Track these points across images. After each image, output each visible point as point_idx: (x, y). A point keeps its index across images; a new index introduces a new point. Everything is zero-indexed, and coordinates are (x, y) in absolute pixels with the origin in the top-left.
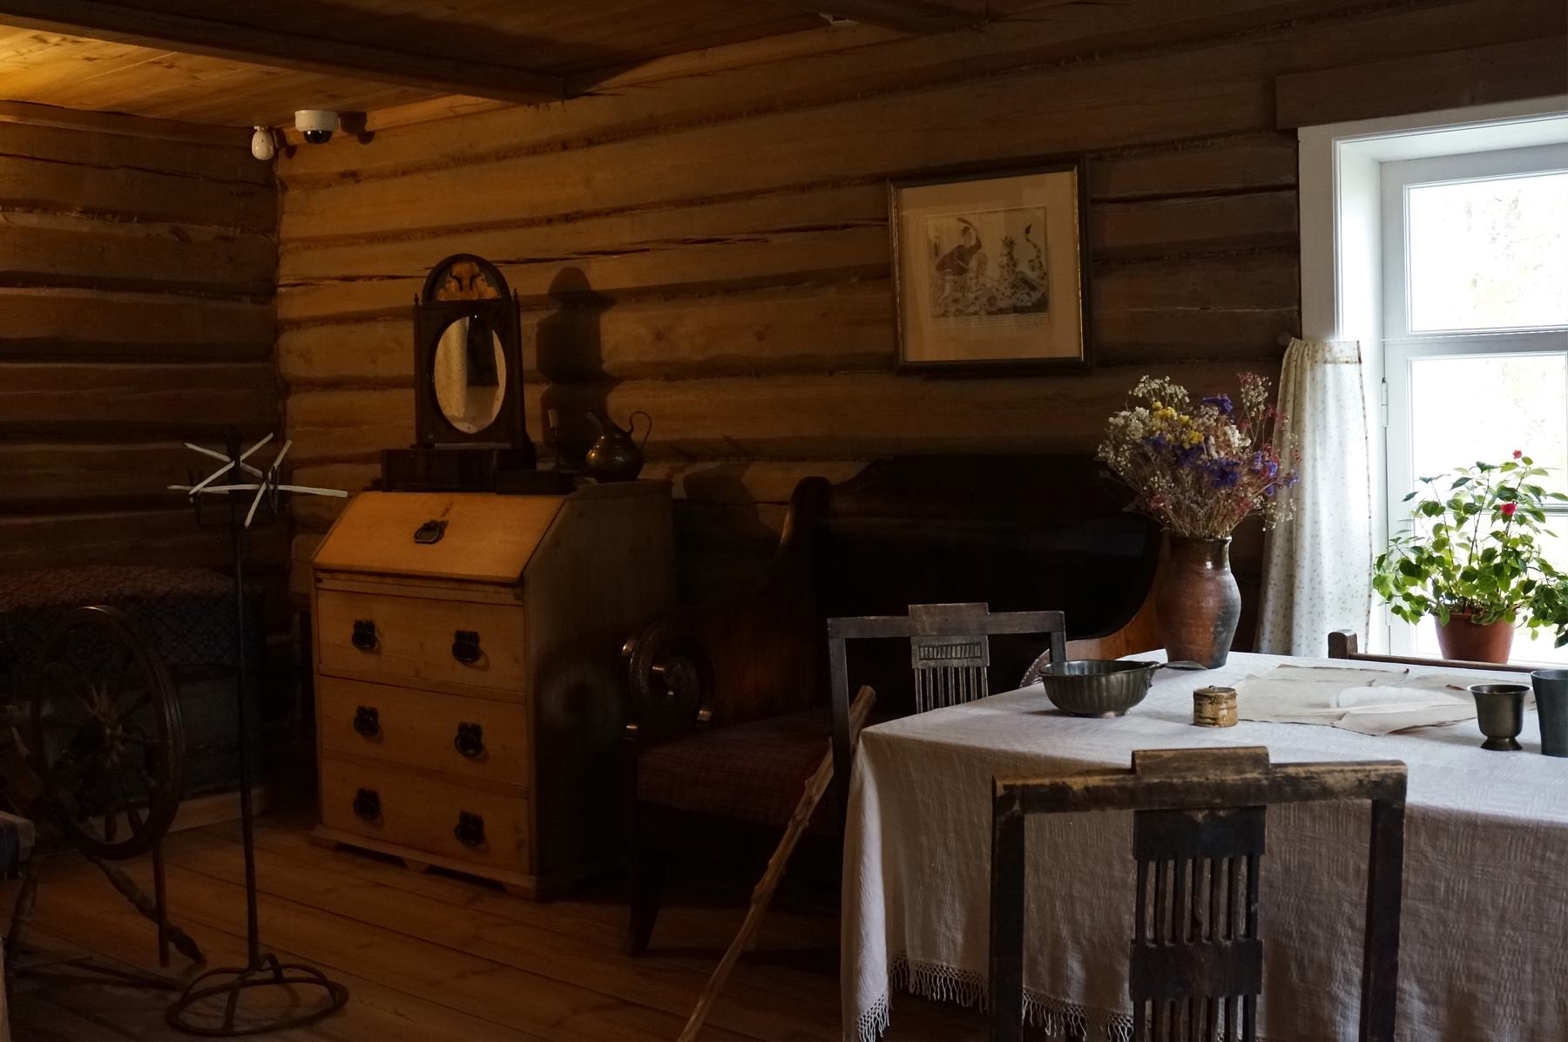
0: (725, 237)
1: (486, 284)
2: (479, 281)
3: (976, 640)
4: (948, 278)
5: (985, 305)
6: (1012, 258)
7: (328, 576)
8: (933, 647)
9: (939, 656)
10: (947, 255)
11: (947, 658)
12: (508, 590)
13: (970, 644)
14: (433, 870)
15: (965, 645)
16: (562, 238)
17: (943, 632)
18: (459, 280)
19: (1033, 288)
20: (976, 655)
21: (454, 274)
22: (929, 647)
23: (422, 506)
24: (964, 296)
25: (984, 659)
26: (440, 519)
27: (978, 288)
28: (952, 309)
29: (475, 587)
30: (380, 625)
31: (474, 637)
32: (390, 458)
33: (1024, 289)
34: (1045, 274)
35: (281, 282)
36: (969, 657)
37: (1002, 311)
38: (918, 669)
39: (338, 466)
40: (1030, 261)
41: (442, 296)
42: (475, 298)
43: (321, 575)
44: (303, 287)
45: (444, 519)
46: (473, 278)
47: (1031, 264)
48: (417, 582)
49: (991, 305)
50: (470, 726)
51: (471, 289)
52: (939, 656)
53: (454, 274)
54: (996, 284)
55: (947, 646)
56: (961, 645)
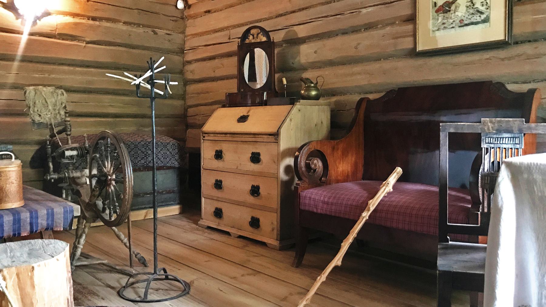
0: (343, 13)
1: (262, 36)
2: (260, 35)
3: (516, 136)
4: (440, 15)
5: (458, 24)
6: (472, 3)
7: (207, 135)
8: (493, 138)
9: (496, 142)
10: (441, 6)
11: (500, 143)
12: (273, 137)
13: (513, 138)
14: (240, 237)
15: (511, 138)
16: (282, 22)
17: (499, 131)
18: (253, 35)
19: (482, 13)
20: (516, 143)
21: (251, 33)
22: (491, 138)
23: (241, 111)
24: (448, 21)
25: (520, 145)
26: (246, 115)
27: (455, 17)
28: (442, 27)
29: (260, 136)
30: (224, 152)
31: (259, 154)
32: (230, 96)
33: (477, 14)
34: (489, 7)
35: (185, 49)
36: (513, 144)
37: (467, 25)
38: (485, 148)
39: (202, 107)
40: (481, 3)
41: (247, 41)
42: (259, 41)
43: (205, 135)
44: (193, 50)
45: (248, 114)
46: (258, 34)
47: (482, 4)
48: (238, 136)
49: (461, 23)
50: (255, 186)
51: (257, 38)
52: (496, 142)
53: (251, 33)
54: (464, 14)
55: (501, 138)
56: (509, 138)
